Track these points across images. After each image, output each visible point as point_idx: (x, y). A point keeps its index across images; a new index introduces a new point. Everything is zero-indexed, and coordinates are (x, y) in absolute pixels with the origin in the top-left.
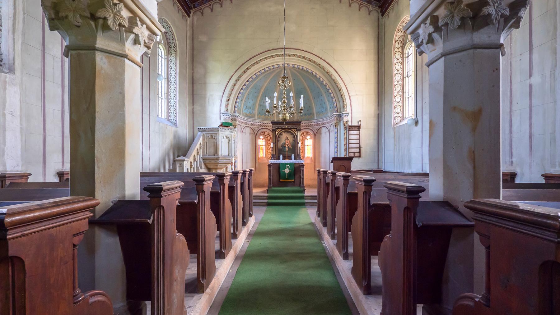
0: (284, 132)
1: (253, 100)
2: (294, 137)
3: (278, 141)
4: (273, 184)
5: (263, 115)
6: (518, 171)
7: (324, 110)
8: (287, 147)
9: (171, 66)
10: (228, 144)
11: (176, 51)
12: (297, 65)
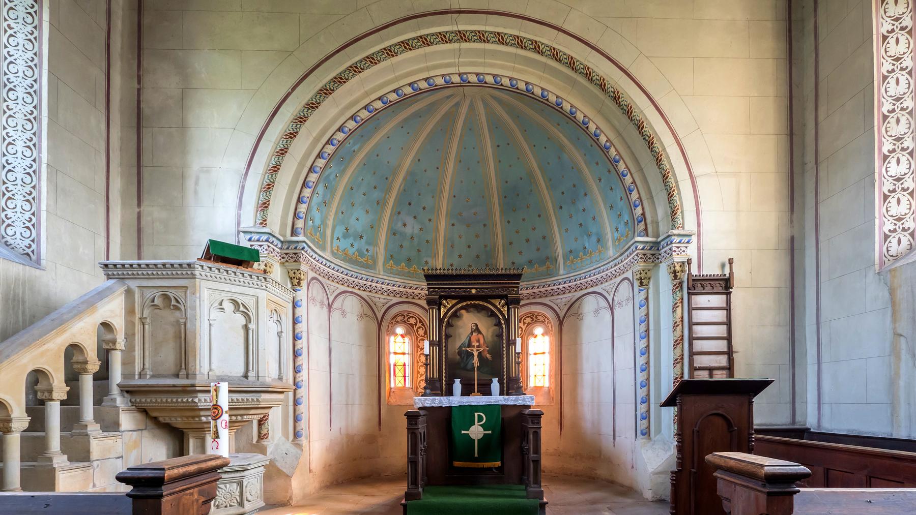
1: (367, 212)
2: (499, 324)
3: (448, 336)
5: (403, 264)
7: (589, 243)
8: (476, 354)
9: (13, 25)
10: (242, 332)
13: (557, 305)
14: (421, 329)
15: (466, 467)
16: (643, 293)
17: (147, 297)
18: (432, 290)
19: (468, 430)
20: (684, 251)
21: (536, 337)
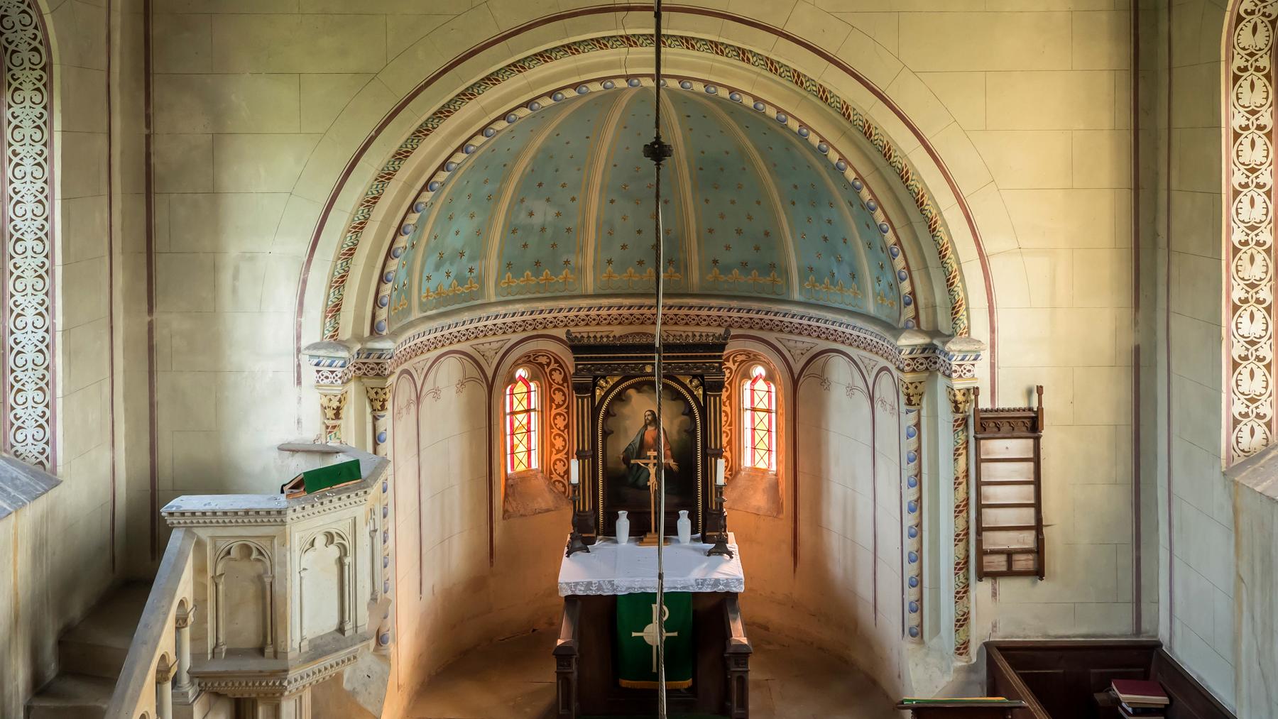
1: (472, 216)
2: (690, 413)
7: (841, 273)
10: (335, 570)
11: (43, 69)
12: (707, 83)
13: (790, 351)
14: (562, 417)
15: (639, 687)
16: (913, 415)
17: (222, 548)
18: (581, 366)
19: (642, 631)
20: (969, 371)
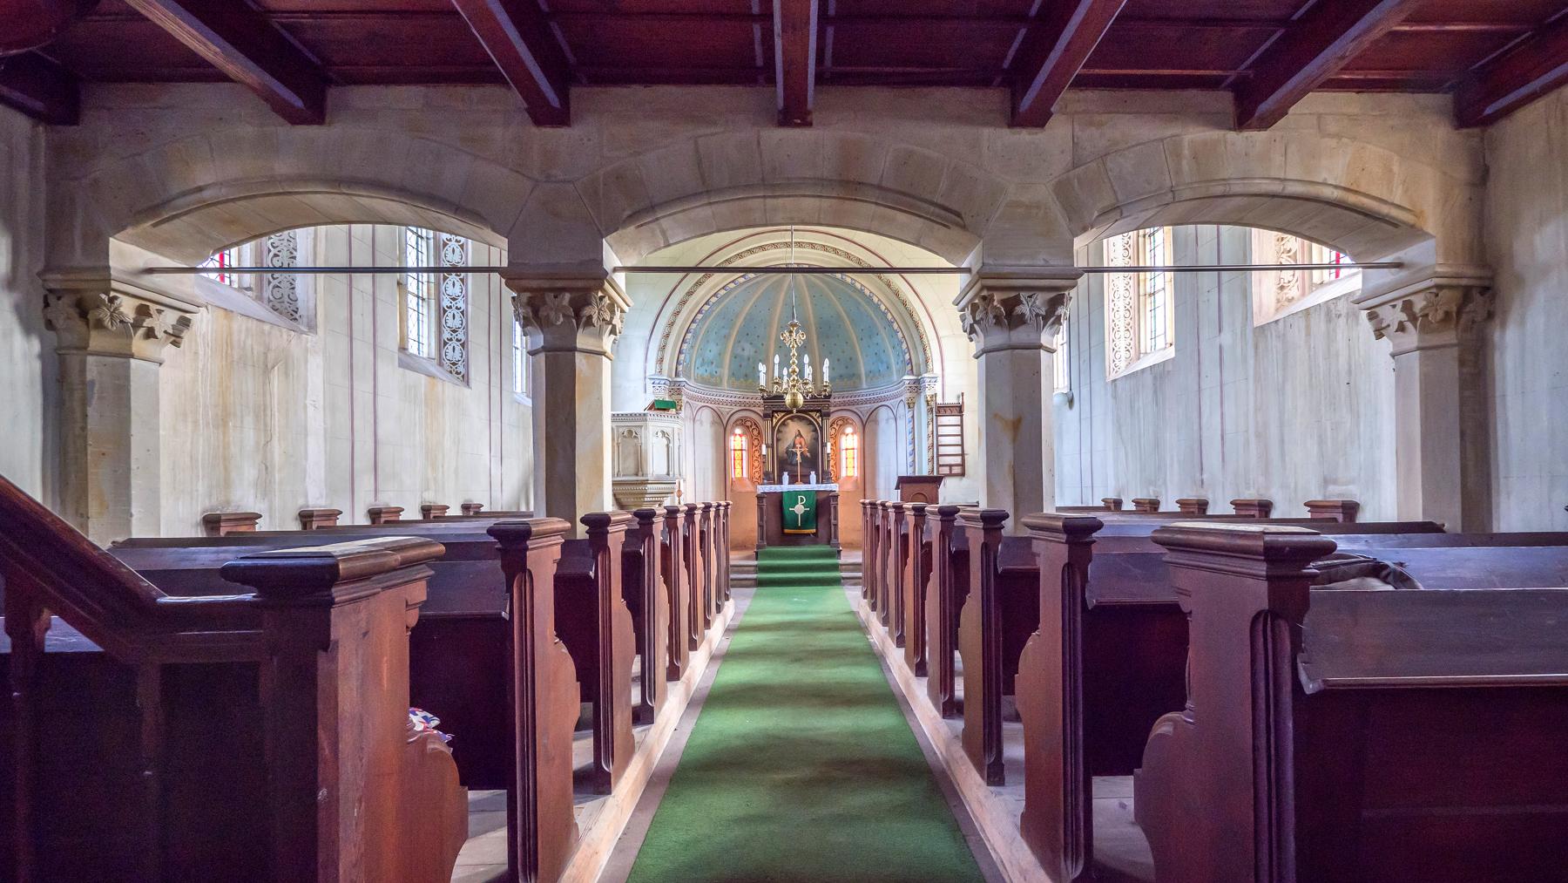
0: (791, 418)
2: (815, 430)
3: (778, 440)
4: (767, 539)
6: (1210, 498)
7: (883, 368)
8: (799, 453)
10: (666, 449)
21: (847, 435)
